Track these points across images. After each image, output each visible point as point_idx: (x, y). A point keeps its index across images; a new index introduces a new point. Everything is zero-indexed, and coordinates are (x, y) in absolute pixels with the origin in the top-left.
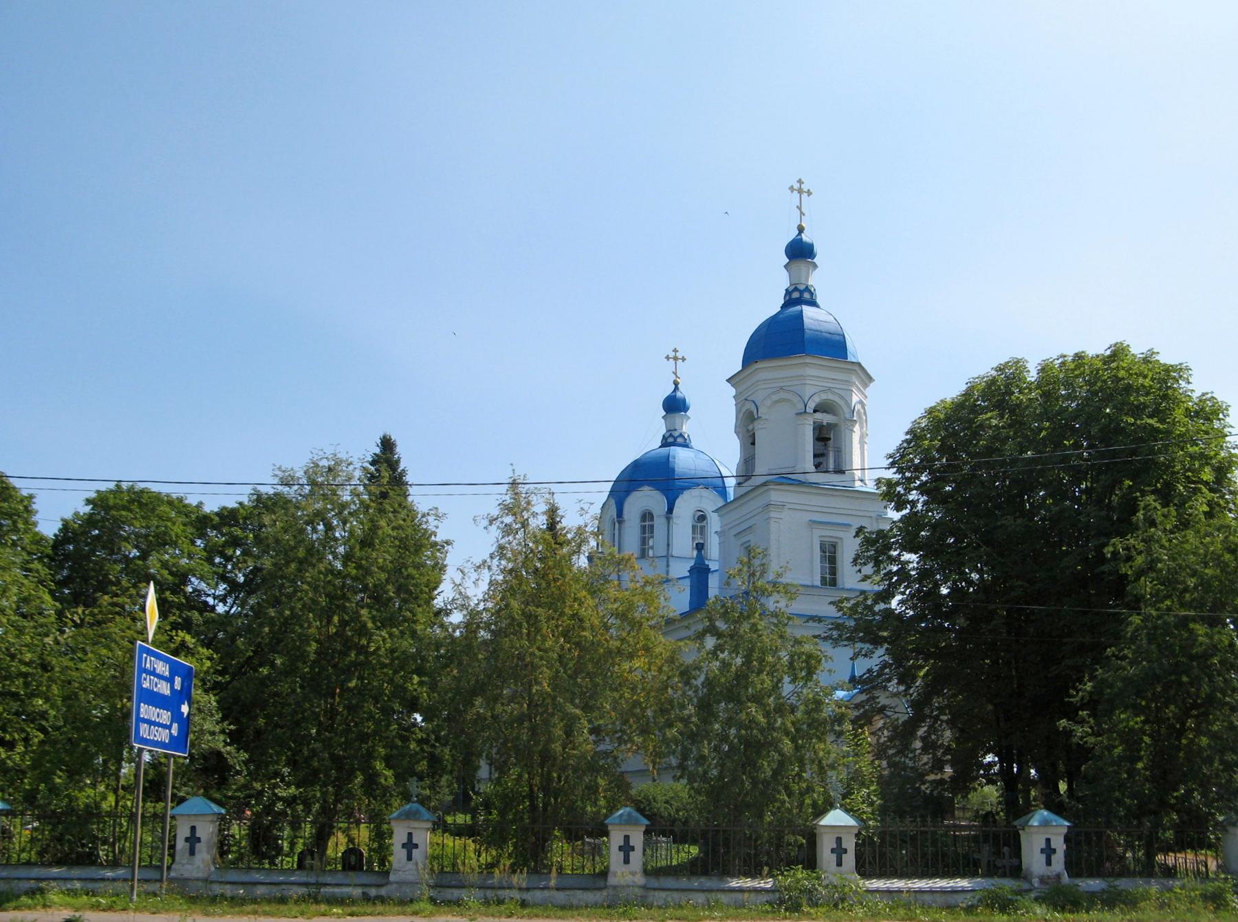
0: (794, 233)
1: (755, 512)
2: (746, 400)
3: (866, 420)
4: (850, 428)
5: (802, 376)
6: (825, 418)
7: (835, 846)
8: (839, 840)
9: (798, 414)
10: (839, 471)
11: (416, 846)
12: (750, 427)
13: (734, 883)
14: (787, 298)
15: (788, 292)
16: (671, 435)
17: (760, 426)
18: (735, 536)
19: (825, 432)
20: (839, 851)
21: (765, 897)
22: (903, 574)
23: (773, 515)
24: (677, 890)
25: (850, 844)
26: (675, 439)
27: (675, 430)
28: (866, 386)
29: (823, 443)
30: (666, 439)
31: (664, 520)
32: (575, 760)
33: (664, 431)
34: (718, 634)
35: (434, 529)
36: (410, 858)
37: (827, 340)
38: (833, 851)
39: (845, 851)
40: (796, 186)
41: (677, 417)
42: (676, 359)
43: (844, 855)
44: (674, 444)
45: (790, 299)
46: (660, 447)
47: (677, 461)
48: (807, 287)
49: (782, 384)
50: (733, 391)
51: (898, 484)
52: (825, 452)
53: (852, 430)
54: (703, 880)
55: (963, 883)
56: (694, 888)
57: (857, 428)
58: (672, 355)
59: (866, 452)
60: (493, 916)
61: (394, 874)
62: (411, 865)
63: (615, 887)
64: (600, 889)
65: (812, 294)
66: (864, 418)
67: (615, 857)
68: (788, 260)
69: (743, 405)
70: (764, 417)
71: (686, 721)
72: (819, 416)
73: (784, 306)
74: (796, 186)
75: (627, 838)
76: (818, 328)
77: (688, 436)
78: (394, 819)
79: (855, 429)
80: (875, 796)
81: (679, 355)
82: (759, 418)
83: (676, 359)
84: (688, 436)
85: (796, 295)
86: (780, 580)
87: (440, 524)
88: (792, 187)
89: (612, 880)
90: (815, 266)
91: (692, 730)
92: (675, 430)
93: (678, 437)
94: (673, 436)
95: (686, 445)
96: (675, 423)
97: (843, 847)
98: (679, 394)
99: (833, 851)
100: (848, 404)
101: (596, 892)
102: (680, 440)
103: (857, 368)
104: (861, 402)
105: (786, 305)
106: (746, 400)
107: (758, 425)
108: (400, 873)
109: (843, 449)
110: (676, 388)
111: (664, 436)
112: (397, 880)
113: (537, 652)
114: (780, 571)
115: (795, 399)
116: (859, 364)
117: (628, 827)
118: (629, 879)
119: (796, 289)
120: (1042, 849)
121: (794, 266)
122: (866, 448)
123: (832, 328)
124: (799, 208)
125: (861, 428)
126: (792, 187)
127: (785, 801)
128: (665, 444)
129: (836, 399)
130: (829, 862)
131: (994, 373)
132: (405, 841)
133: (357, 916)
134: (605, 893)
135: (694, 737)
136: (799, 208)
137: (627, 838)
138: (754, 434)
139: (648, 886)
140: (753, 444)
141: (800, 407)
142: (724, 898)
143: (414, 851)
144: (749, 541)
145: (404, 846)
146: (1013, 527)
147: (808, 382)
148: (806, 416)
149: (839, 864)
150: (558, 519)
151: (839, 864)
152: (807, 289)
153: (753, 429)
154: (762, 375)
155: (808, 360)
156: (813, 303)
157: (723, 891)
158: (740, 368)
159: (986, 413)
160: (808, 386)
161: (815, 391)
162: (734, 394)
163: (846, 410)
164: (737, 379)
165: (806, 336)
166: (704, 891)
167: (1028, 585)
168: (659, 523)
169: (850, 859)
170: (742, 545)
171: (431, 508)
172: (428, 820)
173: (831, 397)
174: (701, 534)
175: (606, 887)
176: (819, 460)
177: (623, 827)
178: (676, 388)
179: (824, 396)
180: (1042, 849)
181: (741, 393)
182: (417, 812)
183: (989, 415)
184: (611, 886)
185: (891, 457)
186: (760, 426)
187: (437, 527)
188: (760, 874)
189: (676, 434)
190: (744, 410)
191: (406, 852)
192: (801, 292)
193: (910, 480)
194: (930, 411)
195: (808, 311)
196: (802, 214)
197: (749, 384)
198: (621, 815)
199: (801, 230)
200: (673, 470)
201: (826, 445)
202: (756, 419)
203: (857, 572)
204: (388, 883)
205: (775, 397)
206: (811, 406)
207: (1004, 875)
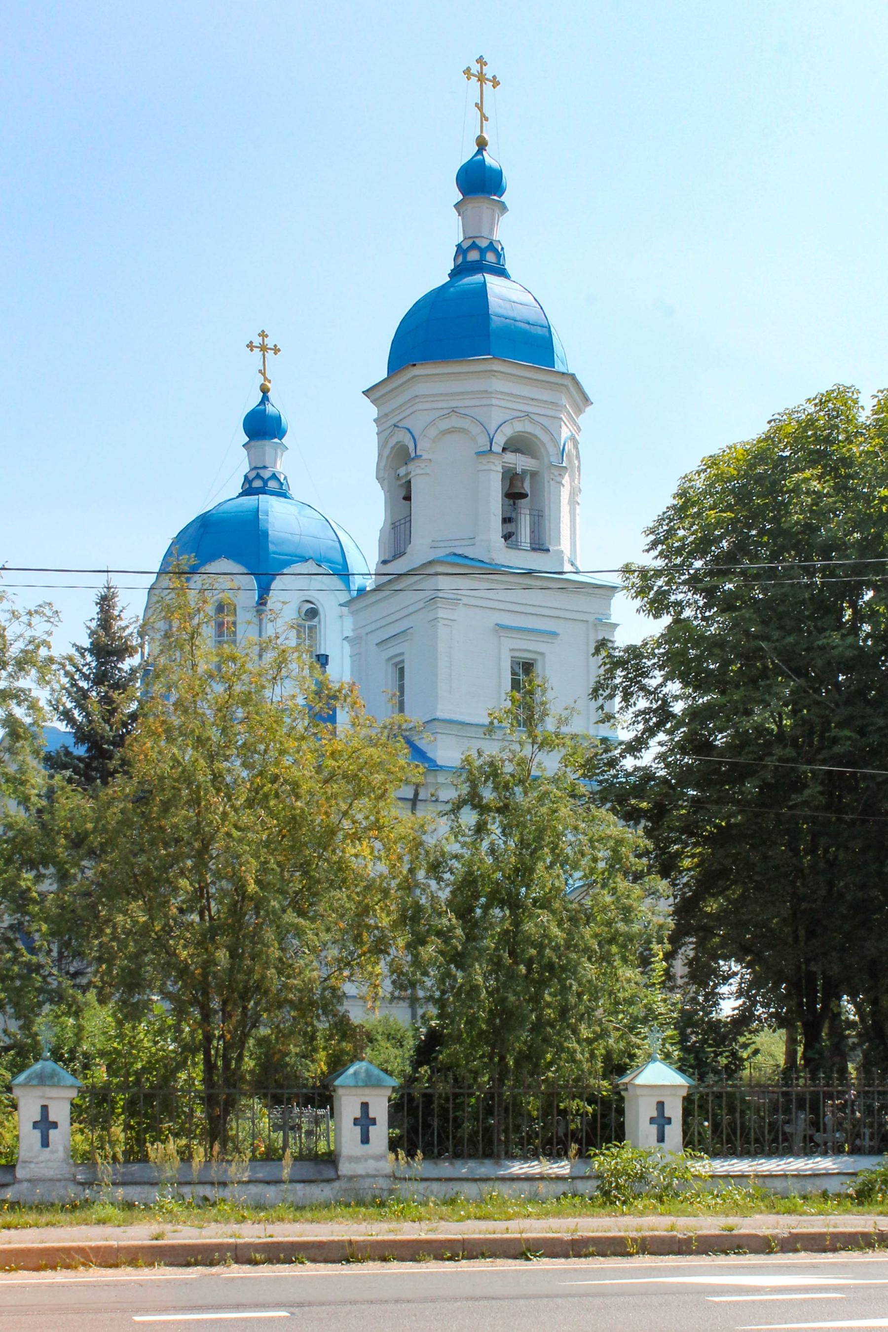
0: (470, 150)
1: (411, 609)
2: (395, 426)
3: (579, 467)
4: (558, 479)
5: (486, 391)
6: (520, 462)
7: (655, 1114)
8: (661, 1105)
9: (480, 454)
10: (539, 546)
11: (55, 1125)
12: (402, 471)
13: (518, 1168)
14: (460, 260)
15: (461, 250)
16: (258, 476)
17: (419, 471)
18: (377, 645)
19: (519, 484)
20: (661, 1121)
21: (561, 1187)
22: (663, 714)
23: (441, 613)
24: (439, 1180)
25: (675, 1111)
26: (265, 482)
27: (265, 467)
28: (579, 411)
29: (511, 502)
30: (250, 482)
31: (250, 615)
32: (298, 994)
33: (247, 469)
34: (482, 808)
35: (45, 637)
36: (45, 1143)
37: (525, 333)
38: (652, 1120)
39: (669, 1121)
40: (475, 68)
41: (269, 445)
42: (263, 348)
43: (667, 1127)
44: (262, 491)
45: (464, 261)
46: (241, 495)
47: (271, 519)
48: (491, 243)
49: (454, 404)
50: (373, 411)
51: (658, 573)
52: (514, 515)
53: (560, 483)
54: (472, 1164)
55: (825, 1164)
56: (461, 1176)
57: (566, 480)
58: (257, 341)
59: (578, 518)
60: (216, 1221)
61: (23, 1168)
62: (46, 1153)
63: (351, 1178)
64: (328, 1181)
65: (498, 255)
66: (576, 462)
67: (350, 1134)
68: (461, 197)
69: (391, 435)
70: (425, 456)
71: (444, 935)
72: (511, 458)
73: (454, 274)
74: (475, 68)
75: (365, 1106)
76: (510, 314)
77: (285, 478)
78: (18, 1085)
79: (563, 482)
80: (672, 1044)
81: (270, 343)
82: (417, 457)
83: (263, 348)
84: (285, 478)
85: (473, 256)
86: (564, 729)
87: (54, 629)
88: (469, 69)
89: (345, 1168)
90: (503, 208)
91: (456, 948)
92: (265, 467)
93: (269, 479)
94: (262, 478)
95: (282, 494)
96: (264, 455)
97: (666, 1115)
98: (270, 409)
99: (356, 1122)
100: (555, 441)
101: (322, 1185)
102: (272, 484)
103: (568, 382)
104: (573, 439)
105: (458, 272)
106: (395, 426)
107: (415, 470)
108: (32, 1166)
109: (547, 513)
110: (265, 399)
111: (246, 477)
112: (28, 1177)
113: (236, 834)
114: (565, 714)
115: (475, 429)
116: (573, 377)
117: (367, 1091)
118: (370, 1166)
119: (474, 246)
120: (355, 1119)
121: (469, 207)
122: (578, 511)
123: (532, 314)
124: (480, 107)
125: (572, 480)
126: (469, 69)
127: (575, 1051)
128: (249, 490)
129: (538, 432)
130: (647, 1137)
131: (811, 409)
132: (38, 1118)
133: (16, 1228)
134: (336, 1185)
135: (459, 959)
136: (480, 107)
137: (365, 1106)
138: (409, 482)
139: (398, 1175)
140: (408, 498)
141: (482, 442)
142: (506, 1189)
143: (52, 1132)
144: (402, 654)
145: (36, 1125)
146: (841, 649)
147: (494, 402)
148: (492, 458)
149: (661, 1139)
150: (116, 613)
151: (661, 1139)
152: (492, 247)
153: (408, 474)
154: (422, 388)
155: (497, 366)
156: (501, 272)
157: (503, 1179)
158: (384, 374)
159: (804, 470)
160: (493, 408)
161: (507, 418)
162: (376, 416)
163: (551, 450)
164: (377, 394)
165: (493, 326)
166: (475, 1180)
167: (858, 737)
168: (244, 616)
169: (674, 1132)
170: (389, 659)
171: (41, 603)
172: (72, 1087)
173: (528, 427)
174: (310, 637)
175: (338, 1178)
176: (510, 527)
177: (360, 1091)
178: (265, 399)
179: (519, 427)
180: (355, 1119)
181: (386, 415)
182: (53, 1075)
183: (807, 473)
184: (345, 1176)
185: (652, 533)
186: (419, 471)
187: (49, 633)
188: (566, 1154)
189: (266, 474)
190: (393, 441)
191: (359, 1131)
192: (483, 251)
193: (678, 568)
194: (713, 462)
195: (493, 283)
196: (484, 118)
197: (399, 400)
198: (355, 1074)
199: (482, 144)
200: (266, 534)
201: (514, 504)
202: (413, 459)
203: (598, 709)
204: (15, 1181)
205: (444, 425)
206: (500, 440)
207: (825, 1154)
